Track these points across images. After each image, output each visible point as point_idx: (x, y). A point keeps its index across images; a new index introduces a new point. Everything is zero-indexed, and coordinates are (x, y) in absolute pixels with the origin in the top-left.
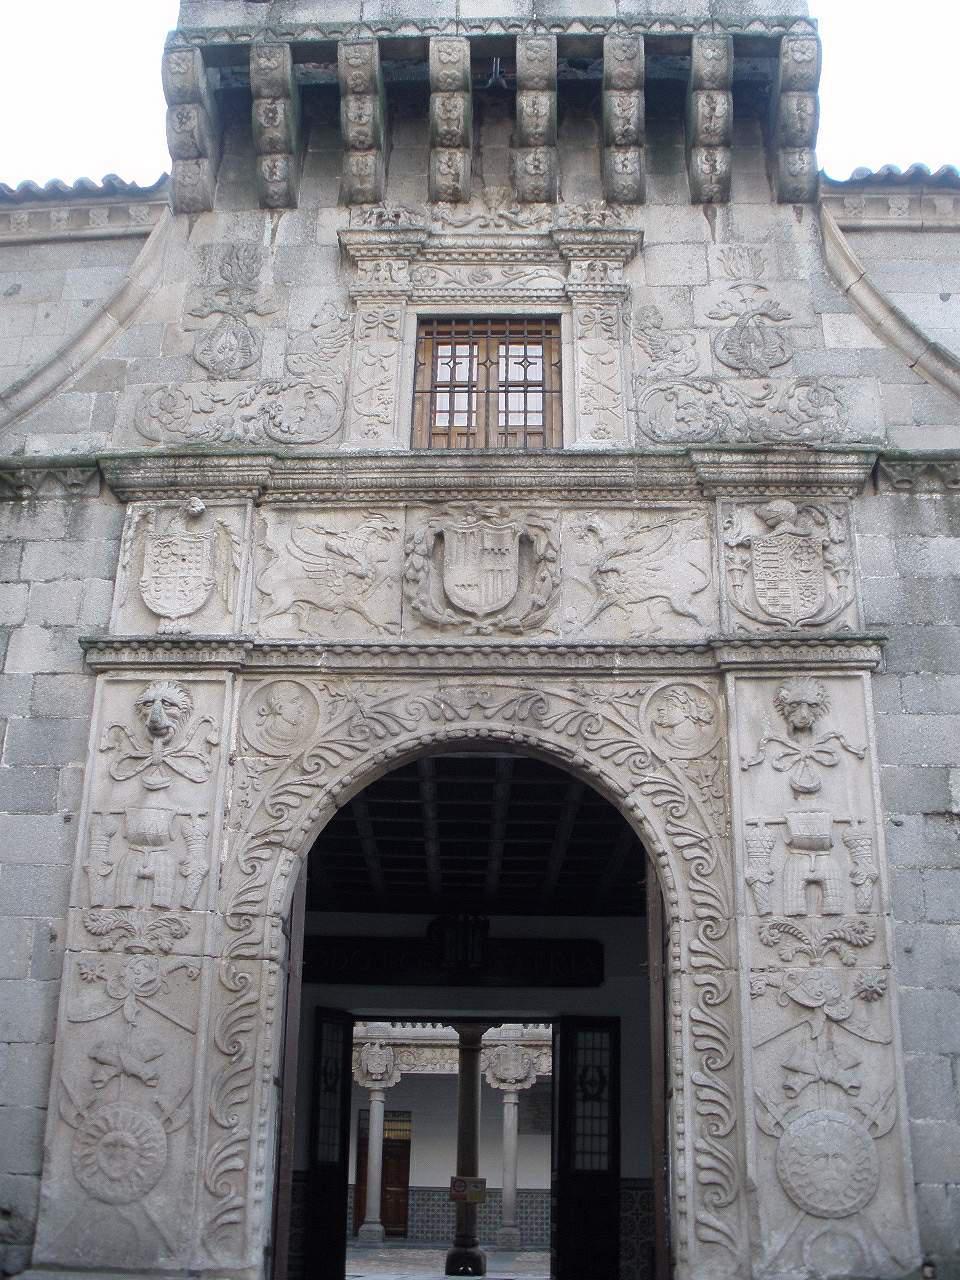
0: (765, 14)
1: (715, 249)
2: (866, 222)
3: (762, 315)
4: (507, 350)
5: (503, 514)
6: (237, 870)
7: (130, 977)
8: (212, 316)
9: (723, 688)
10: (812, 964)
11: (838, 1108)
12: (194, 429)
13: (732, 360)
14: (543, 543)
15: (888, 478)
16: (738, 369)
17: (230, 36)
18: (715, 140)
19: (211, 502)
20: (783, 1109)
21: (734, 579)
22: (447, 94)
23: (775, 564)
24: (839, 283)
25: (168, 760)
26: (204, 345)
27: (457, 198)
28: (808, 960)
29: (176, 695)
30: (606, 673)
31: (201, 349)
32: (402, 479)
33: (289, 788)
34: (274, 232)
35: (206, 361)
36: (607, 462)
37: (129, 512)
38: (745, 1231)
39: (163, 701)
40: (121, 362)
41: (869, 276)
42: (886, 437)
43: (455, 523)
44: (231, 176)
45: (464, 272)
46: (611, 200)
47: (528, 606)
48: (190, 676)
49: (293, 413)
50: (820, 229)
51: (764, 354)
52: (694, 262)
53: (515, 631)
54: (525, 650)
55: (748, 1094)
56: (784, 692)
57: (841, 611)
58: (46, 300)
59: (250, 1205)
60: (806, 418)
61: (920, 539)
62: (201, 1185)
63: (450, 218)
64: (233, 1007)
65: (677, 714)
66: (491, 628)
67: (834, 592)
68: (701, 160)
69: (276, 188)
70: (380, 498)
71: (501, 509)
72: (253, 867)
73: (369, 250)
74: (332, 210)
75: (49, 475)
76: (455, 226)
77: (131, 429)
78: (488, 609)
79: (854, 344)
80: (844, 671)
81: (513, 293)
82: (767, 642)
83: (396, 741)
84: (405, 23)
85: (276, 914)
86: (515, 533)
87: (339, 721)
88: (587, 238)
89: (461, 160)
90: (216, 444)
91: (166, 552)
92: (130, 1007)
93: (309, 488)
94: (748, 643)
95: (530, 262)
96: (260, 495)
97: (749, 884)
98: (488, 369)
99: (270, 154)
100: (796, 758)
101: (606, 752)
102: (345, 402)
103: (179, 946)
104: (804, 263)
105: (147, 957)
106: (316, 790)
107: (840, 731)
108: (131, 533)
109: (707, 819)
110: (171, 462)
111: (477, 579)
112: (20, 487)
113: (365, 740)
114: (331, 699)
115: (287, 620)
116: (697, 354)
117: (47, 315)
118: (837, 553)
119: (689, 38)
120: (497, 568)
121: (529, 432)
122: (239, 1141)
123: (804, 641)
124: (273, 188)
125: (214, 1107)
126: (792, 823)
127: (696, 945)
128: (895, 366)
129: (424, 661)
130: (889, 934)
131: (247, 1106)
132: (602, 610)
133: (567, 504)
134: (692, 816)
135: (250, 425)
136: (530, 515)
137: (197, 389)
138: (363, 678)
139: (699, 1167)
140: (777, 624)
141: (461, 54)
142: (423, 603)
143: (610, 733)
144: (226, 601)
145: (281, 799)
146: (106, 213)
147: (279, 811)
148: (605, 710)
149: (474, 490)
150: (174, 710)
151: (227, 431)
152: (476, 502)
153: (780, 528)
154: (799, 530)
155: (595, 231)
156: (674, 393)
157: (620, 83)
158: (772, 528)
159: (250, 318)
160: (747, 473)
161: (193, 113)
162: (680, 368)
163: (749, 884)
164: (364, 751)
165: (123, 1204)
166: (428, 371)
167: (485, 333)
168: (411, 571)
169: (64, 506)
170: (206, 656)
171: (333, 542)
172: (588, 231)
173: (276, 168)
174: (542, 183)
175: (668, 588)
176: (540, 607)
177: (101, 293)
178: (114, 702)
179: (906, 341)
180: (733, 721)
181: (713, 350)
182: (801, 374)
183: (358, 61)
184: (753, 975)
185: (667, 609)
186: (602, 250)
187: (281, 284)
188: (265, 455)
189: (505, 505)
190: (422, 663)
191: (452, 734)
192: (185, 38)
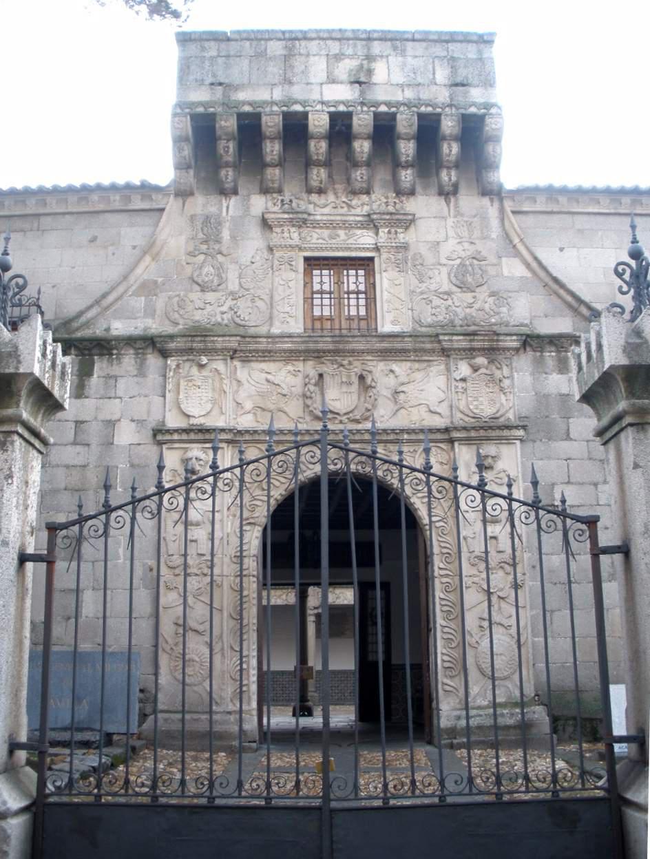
1: (450, 221)
2: (525, 209)
3: (473, 258)
4: (348, 273)
5: (350, 363)
9: (453, 448)
11: (503, 635)
12: (197, 318)
16: (460, 288)
17: (205, 108)
18: (452, 165)
20: (479, 636)
24: (511, 242)
27: (320, 191)
32: (302, 347)
34: (228, 208)
36: (399, 339)
37: (169, 362)
39: (196, 458)
41: (525, 240)
42: (531, 323)
43: (328, 369)
46: (399, 193)
47: (364, 410)
50: (502, 210)
51: (473, 279)
52: (439, 228)
53: (358, 422)
57: (507, 411)
58: (112, 245)
61: (545, 376)
63: (318, 203)
68: (444, 175)
69: (229, 185)
70: (291, 356)
71: (349, 361)
75: (127, 344)
76: (324, 207)
78: (344, 411)
80: (508, 441)
81: (350, 246)
82: (473, 428)
84: (296, 102)
85: (254, 556)
86: (356, 374)
88: (388, 217)
89: (323, 173)
91: (190, 384)
93: (257, 351)
94: (465, 428)
95: (359, 228)
96: (233, 354)
97: (465, 538)
102: (271, 304)
104: (494, 229)
105: (197, 577)
108: (171, 374)
110: (190, 339)
111: (340, 398)
112: (112, 349)
115: (250, 417)
117: (113, 254)
118: (506, 383)
119: (439, 115)
121: (360, 319)
123: (491, 428)
124: (227, 186)
125: (232, 642)
127: (442, 566)
130: (525, 560)
132: (397, 411)
133: (380, 358)
134: (439, 507)
135: (225, 316)
137: (195, 295)
139: (443, 661)
142: (315, 409)
144: (221, 408)
146: (139, 197)
149: (336, 352)
150: (201, 462)
151: (213, 320)
154: (488, 372)
155: (391, 214)
157: (405, 137)
158: (476, 371)
159: (219, 256)
160: (464, 344)
162: (433, 287)
165: (195, 685)
169: (135, 358)
171: (269, 377)
172: (388, 214)
173: (228, 175)
175: (427, 400)
176: (369, 410)
177: (141, 242)
179: (542, 274)
181: (449, 278)
182: (492, 290)
183: (272, 123)
189: (351, 359)
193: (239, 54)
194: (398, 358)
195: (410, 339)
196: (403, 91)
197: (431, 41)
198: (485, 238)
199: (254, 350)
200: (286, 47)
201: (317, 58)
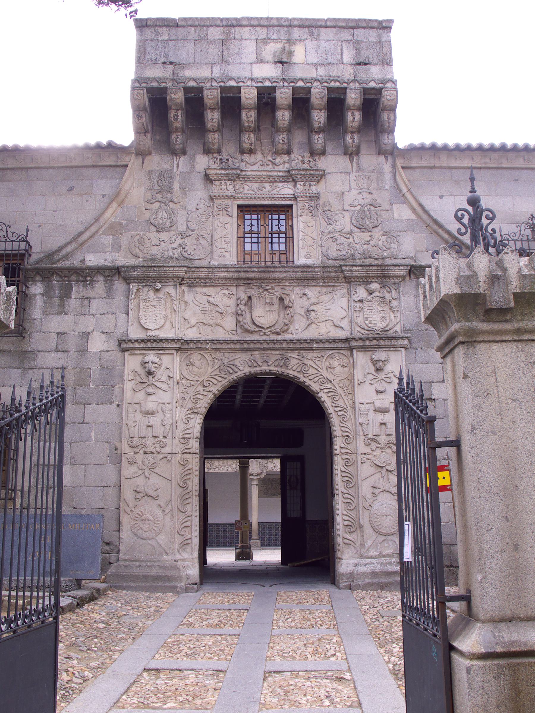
0: (376, 77)
1: (353, 176)
3: (370, 205)
4: (272, 217)
6: (182, 422)
7: (147, 462)
8: (156, 203)
9: (352, 354)
10: (382, 452)
12: (153, 253)
13: (358, 225)
14: (288, 300)
15: (414, 274)
16: (360, 229)
18: (354, 130)
19: (163, 284)
21: (356, 314)
22: (248, 110)
23: (371, 308)
24: (401, 191)
25: (154, 383)
26: (154, 217)
27: (251, 152)
28: (381, 450)
29: (156, 359)
30: (311, 349)
31: (153, 218)
32: (236, 275)
33: (199, 392)
34: (178, 165)
35: (156, 224)
37: (131, 287)
38: (359, 540)
39: (152, 362)
40: (120, 222)
43: (254, 292)
44: (158, 138)
45: (255, 186)
46: (313, 153)
48: (161, 352)
49: (192, 247)
50: (394, 166)
52: (344, 181)
53: (278, 334)
54: (282, 341)
55: (360, 495)
56: (374, 356)
57: (395, 325)
58: (86, 194)
59: (193, 537)
60: (385, 249)
62: (176, 532)
64: (184, 471)
65: (335, 363)
66: (269, 333)
67: (392, 318)
70: (225, 283)
71: (272, 287)
72: (188, 421)
73: (218, 177)
74: (201, 155)
77: (128, 252)
78: (268, 326)
79: (405, 217)
80: (395, 348)
81: (274, 196)
83: (237, 375)
84: (231, 79)
86: (277, 297)
87: (216, 367)
88: (303, 173)
90: (163, 259)
91: (148, 304)
92: (147, 472)
93: (200, 279)
94: (361, 339)
97: (360, 424)
98: (265, 227)
99: (175, 132)
100: (378, 380)
101: (311, 378)
103: (163, 450)
104: (388, 182)
106: (209, 393)
107: (393, 370)
108: (133, 296)
109: (346, 401)
111: (264, 315)
113: (226, 374)
114: (212, 360)
116: (345, 222)
117: (87, 201)
118: (394, 303)
119: (345, 89)
120: (272, 310)
122: (189, 516)
126: (376, 403)
127: (343, 445)
128: (420, 227)
129: (245, 346)
131: (190, 505)
132: (309, 325)
133: (296, 284)
134: (341, 400)
135: (175, 251)
136: (282, 289)
137: (153, 235)
138: (224, 352)
140: (372, 331)
141: (254, 95)
143: (312, 371)
144: (172, 323)
145: (197, 396)
147: (196, 401)
148: (310, 363)
150: (156, 365)
151: (166, 254)
152: (262, 284)
153: (374, 295)
156: (336, 239)
158: (371, 294)
159: (171, 204)
160: (363, 274)
161: (143, 116)
162: (338, 228)
163: (360, 424)
164: (226, 378)
166: (241, 227)
167: (263, 211)
168: (240, 311)
170: (166, 345)
171: (210, 299)
172: (303, 170)
174: (285, 147)
176: (287, 325)
178: (133, 362)
179: (425, 217)
180: (355, 367)
184: (362, 456)
185: (332, 324)
186: (309, 177)
187: (182, 189)
188: (183, 266)
189: (273, 285)
190: (245, 346)
191: (256, 372)
192: (139, 83)
193: (185, 38)
194: (310, 284)
195: (320, 269)
196: (317, 69)
197: (340, 27)
198: (380, 189)
199: (198, 278)
200: (224, 32)
201: (248, 41)
